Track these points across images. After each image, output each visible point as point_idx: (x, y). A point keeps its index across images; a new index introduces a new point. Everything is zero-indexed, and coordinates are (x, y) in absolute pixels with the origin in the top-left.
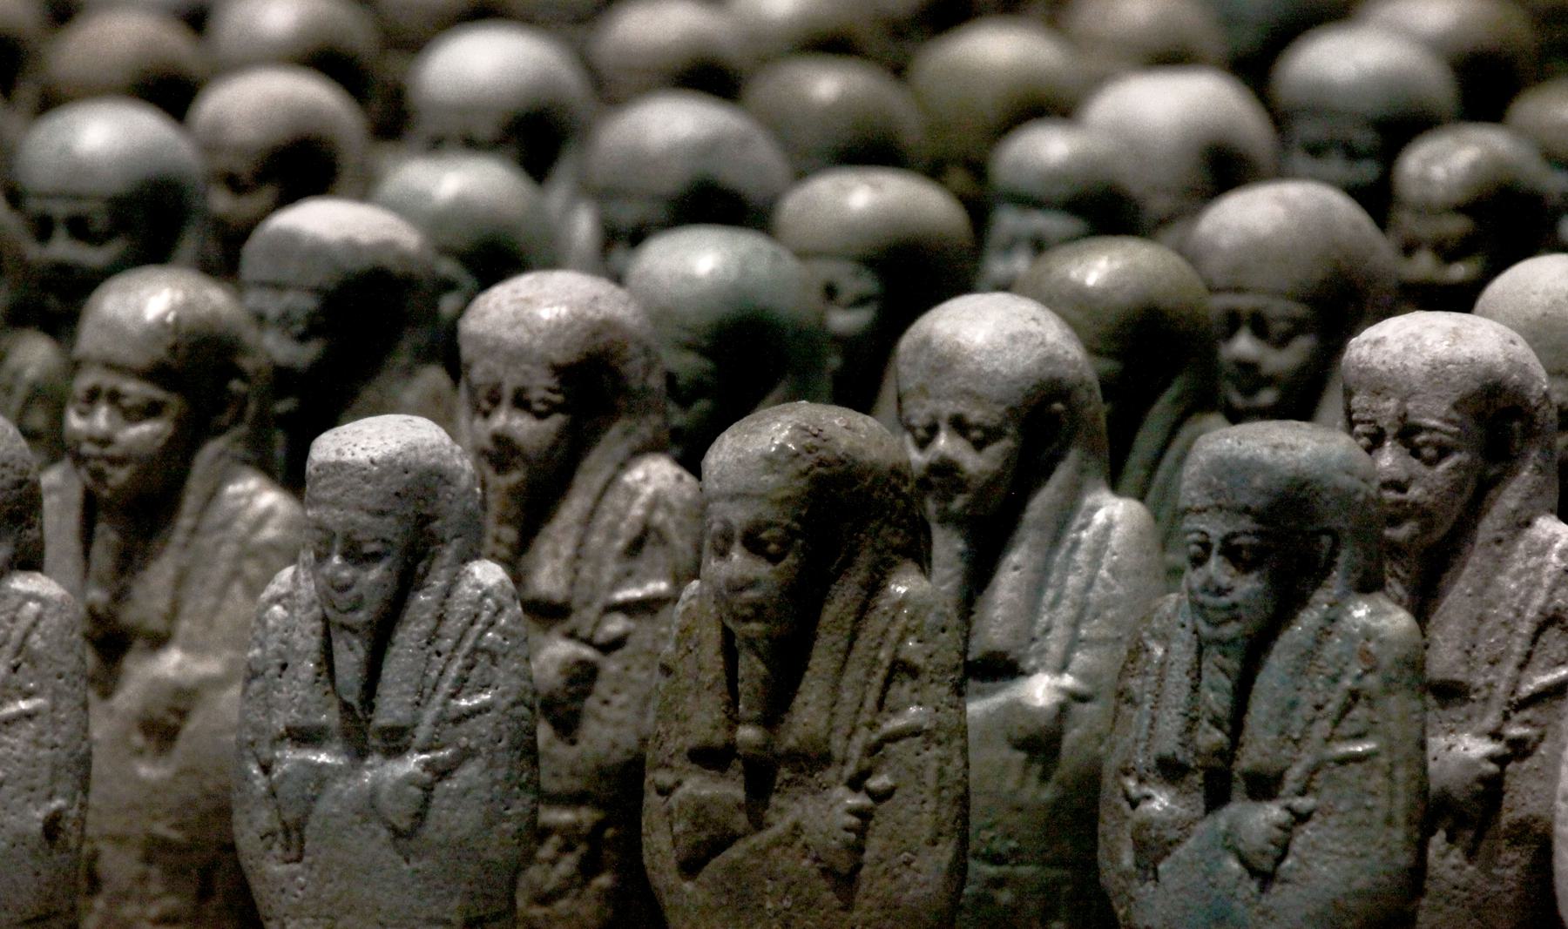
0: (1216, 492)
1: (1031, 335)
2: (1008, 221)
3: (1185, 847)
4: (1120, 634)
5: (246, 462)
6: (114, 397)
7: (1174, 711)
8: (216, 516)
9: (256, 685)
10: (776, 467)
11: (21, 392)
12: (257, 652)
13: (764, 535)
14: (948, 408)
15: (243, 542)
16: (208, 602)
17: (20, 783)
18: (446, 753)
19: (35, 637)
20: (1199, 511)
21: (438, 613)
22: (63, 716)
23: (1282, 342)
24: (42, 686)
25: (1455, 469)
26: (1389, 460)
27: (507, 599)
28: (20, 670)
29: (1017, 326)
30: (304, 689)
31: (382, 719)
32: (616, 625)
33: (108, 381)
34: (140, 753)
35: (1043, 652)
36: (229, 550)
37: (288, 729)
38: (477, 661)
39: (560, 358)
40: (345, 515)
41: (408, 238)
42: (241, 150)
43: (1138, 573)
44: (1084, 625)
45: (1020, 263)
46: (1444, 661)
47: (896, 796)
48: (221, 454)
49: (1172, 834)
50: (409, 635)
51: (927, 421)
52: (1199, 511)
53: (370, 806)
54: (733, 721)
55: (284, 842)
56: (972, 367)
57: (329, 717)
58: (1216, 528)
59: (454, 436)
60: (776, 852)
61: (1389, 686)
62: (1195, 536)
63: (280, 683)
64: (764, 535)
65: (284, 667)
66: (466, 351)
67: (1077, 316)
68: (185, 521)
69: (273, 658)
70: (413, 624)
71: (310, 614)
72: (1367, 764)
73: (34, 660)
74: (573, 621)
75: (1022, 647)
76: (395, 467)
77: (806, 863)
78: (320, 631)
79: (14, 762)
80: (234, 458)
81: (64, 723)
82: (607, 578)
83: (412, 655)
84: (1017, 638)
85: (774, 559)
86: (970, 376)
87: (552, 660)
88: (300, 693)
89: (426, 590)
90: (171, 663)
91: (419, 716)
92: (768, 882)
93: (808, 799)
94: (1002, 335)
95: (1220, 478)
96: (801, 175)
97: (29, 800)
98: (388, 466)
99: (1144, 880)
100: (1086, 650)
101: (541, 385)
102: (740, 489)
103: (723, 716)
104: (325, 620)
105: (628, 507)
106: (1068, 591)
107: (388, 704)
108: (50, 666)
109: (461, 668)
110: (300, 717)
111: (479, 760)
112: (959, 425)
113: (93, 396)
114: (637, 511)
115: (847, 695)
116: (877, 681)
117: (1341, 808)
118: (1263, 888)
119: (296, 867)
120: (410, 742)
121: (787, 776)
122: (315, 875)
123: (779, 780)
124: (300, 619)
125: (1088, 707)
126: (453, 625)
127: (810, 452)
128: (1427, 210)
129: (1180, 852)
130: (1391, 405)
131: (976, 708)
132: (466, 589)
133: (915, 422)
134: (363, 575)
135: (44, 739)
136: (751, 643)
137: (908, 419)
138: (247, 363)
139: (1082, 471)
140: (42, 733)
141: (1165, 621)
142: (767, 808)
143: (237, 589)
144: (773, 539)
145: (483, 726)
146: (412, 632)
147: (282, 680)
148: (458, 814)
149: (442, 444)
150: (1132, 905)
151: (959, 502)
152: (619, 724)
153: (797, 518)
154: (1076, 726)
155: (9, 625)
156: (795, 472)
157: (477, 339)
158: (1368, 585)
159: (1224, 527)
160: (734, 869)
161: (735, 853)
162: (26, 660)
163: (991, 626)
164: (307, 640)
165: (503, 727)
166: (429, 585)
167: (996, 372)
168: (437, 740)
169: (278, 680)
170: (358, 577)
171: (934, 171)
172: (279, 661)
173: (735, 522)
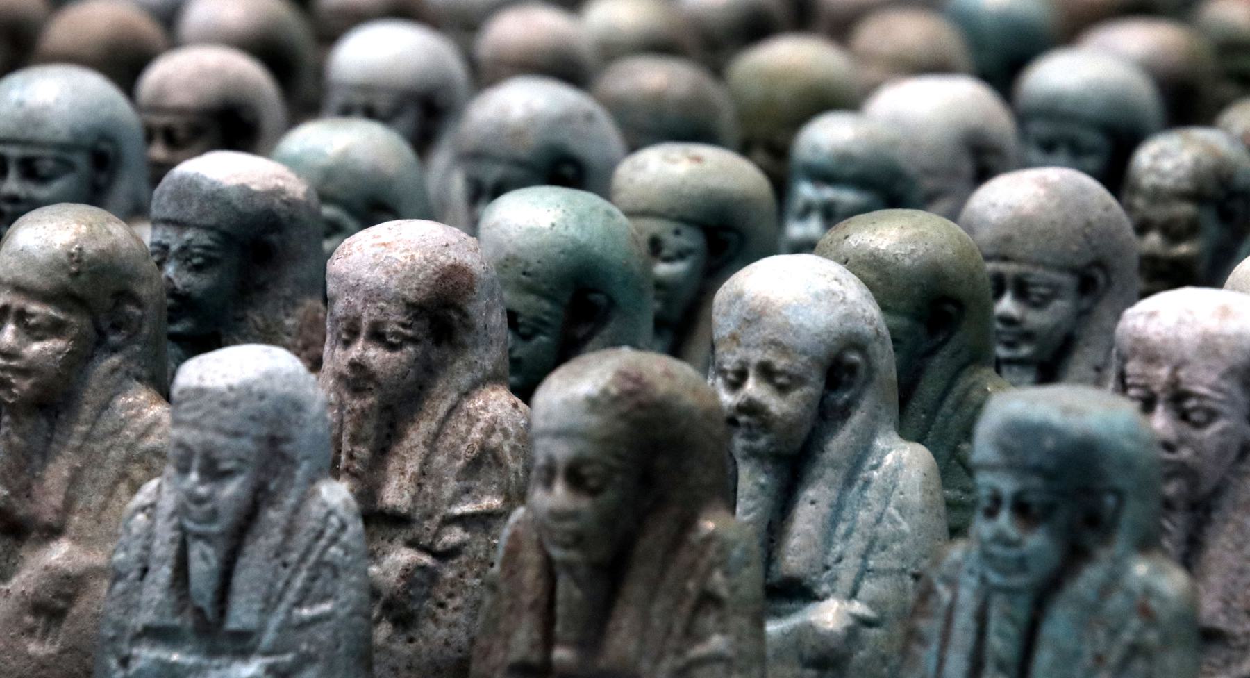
0: (1005, 449)
1: (834, 294)
2: (806, 191)
4: (904, 566)
5: (139, 378)
6: (21, 316)
8: (107, 424)
9: (120, 586)
14: (756, 356)
15: (130, 447)
18: (289, 658)
23: (1041, 304)
25: (1223, 433)
26: (1161, 422)
27: (349, 517)
29: (822, 285)
31: (232, 625)
32: (455, 535)
33: (17, 302)
34: (30, 631)
35: (834, 580)
39: (411, 296)
41: (297, 188)
42: (180, 111)
43: (923, 512)
44: (872, 556)
45: (811, 227)
46: (1210, 609)
48: (114, 370)
51: (737, 367)
54: (548, 641)
56: (779, 320)
57: (185, 621)
58: (1007, 486)
59: (315, 365)
61: (1166, 642)
66: (331, 288)
67: (872, 276)
74: (416, 530)
75: (815, 574)
82: (447, 494)
84: (811, 566)
85: (594, 492)
86: (778, 329)
87: (396, 564)
90: (59, 554)
94: (808, 293)
96: (634, 147)
98: (244, 394)
100: (873, 580)
101: (394, 321)
104: (181, 528)
105: (469, 431)
106: (859, 525)
112: (766, 372)
114: (476, 435)
115: (657, 622)
116: (685, 609)
125: (873, 632)
126: (301, 540)
128: (1158, 196)
130: (1164, 373)
131: (773, 628)
132: (315, 509)
133: (726, 366)
136: (569, 567)
137: (721, 364)
138: (143, 291)
139: (875, 417)
149: (297, 374)
151: (762, 442)
152: (454, 624)
153: (618, 457)
154: (862, 648)
157: (340, 278)
158: (1146, 544)
163: (789, 554)
164: (163, 548)
167: (801, 326)
171: (745, 149)
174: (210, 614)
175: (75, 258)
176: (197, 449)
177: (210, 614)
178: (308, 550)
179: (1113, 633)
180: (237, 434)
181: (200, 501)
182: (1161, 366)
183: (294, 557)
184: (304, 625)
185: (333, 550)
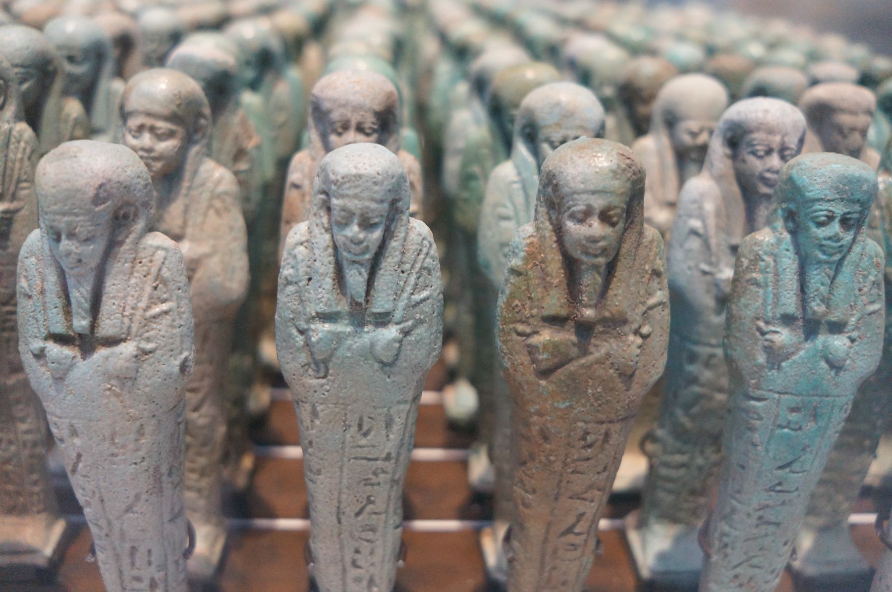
3: (798, 356)
6: (152, 129)
7: (792, 293)
8: (198, 180)
10: (618, 176)
11: (71, 123)
12: (291, 271)
13: (612, 213)
16: (199, 219)
17: (165, 348)
19: (164, 270)
20: (829, 201)
21: (402, 251)
22: (183, 309)
24: (171, 296)
28: (158, 288)
30: (327, 293)
33: (149, 121)
36: (206, 196)
37: (317, 313)
38: (422, 274)
40: (362, 204)
47: (652, 336)
48: (198, 153)
49: (792, 350)
50: (389, 263)
52: (829, 201)
53: (370, 352)
55: (315, 368)
57: (343, 307)
60: (596, 366)
62: (825, 213)
63: (309, 289)
64: (612, 213)
65: (310, 279)
68: (186, 184)
69: (304, 275)
70: (390, 258)
71: (326, 253)
72: (877, 314)
73: (165, 282)
76: (388, 176)
77: (611, 371)
78: (333, 262)
79: (161, 338)
80: (203, 154)
81: (184, 313)
83: (391, 275)
85: (613, 225)
88: (326, 296)
89: (395, 239)
91: (396, 305)
92: (590, 380)
93: (612, 340)
95: (844, 185)
97: (171, 356)
99: (772, 368)
102: (599, 188)
103: (566, 301)
107: (380, 301)
108: (174, 284)
109: (415, 279)
110: (326, 308)
111: (425, 325)
113: (141, 128)
117: (868, 335)
118: (837, 374)
119: (324, 381)
120: (391, 319)
121: (601, 329)
122: (336, 385)
123: (596, 331)
124: (320, 256)
126: (410, 256)
127: (630, 168)
129: (795, 358)
134: (370, 235)
135: (176, 324)
140: (174, 320)
141: (771, 247)
142: (589, 345)
143: (211, 213)
144: (616, 215)
145: (426, 308)
146: (390, 263)
147: (309, 287)
148: (415, 352)
150: (762, 379)
155: (149, 264)
156: (626, 179)
159: (844, 209)
160: (572, 376)
161: (572, 367)
162: (160, 283)
164: (325, 265)
165: (435, 306)
166: (397, 236)
168: (405, 317)
169: (307, 287)
170: (367, 237)
172: (307, 277)
173: (596, 206)
174: (361, 300)
175: (178, 97)
176: (358, 212)
177: (361, 300)
178: (415, 261)
179: (865, 277)
180: (382, 201)
181: (360, 242)
182: (775, 135)
183: (407, 267)
184: (418, 304)
185: (428, 260)
